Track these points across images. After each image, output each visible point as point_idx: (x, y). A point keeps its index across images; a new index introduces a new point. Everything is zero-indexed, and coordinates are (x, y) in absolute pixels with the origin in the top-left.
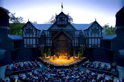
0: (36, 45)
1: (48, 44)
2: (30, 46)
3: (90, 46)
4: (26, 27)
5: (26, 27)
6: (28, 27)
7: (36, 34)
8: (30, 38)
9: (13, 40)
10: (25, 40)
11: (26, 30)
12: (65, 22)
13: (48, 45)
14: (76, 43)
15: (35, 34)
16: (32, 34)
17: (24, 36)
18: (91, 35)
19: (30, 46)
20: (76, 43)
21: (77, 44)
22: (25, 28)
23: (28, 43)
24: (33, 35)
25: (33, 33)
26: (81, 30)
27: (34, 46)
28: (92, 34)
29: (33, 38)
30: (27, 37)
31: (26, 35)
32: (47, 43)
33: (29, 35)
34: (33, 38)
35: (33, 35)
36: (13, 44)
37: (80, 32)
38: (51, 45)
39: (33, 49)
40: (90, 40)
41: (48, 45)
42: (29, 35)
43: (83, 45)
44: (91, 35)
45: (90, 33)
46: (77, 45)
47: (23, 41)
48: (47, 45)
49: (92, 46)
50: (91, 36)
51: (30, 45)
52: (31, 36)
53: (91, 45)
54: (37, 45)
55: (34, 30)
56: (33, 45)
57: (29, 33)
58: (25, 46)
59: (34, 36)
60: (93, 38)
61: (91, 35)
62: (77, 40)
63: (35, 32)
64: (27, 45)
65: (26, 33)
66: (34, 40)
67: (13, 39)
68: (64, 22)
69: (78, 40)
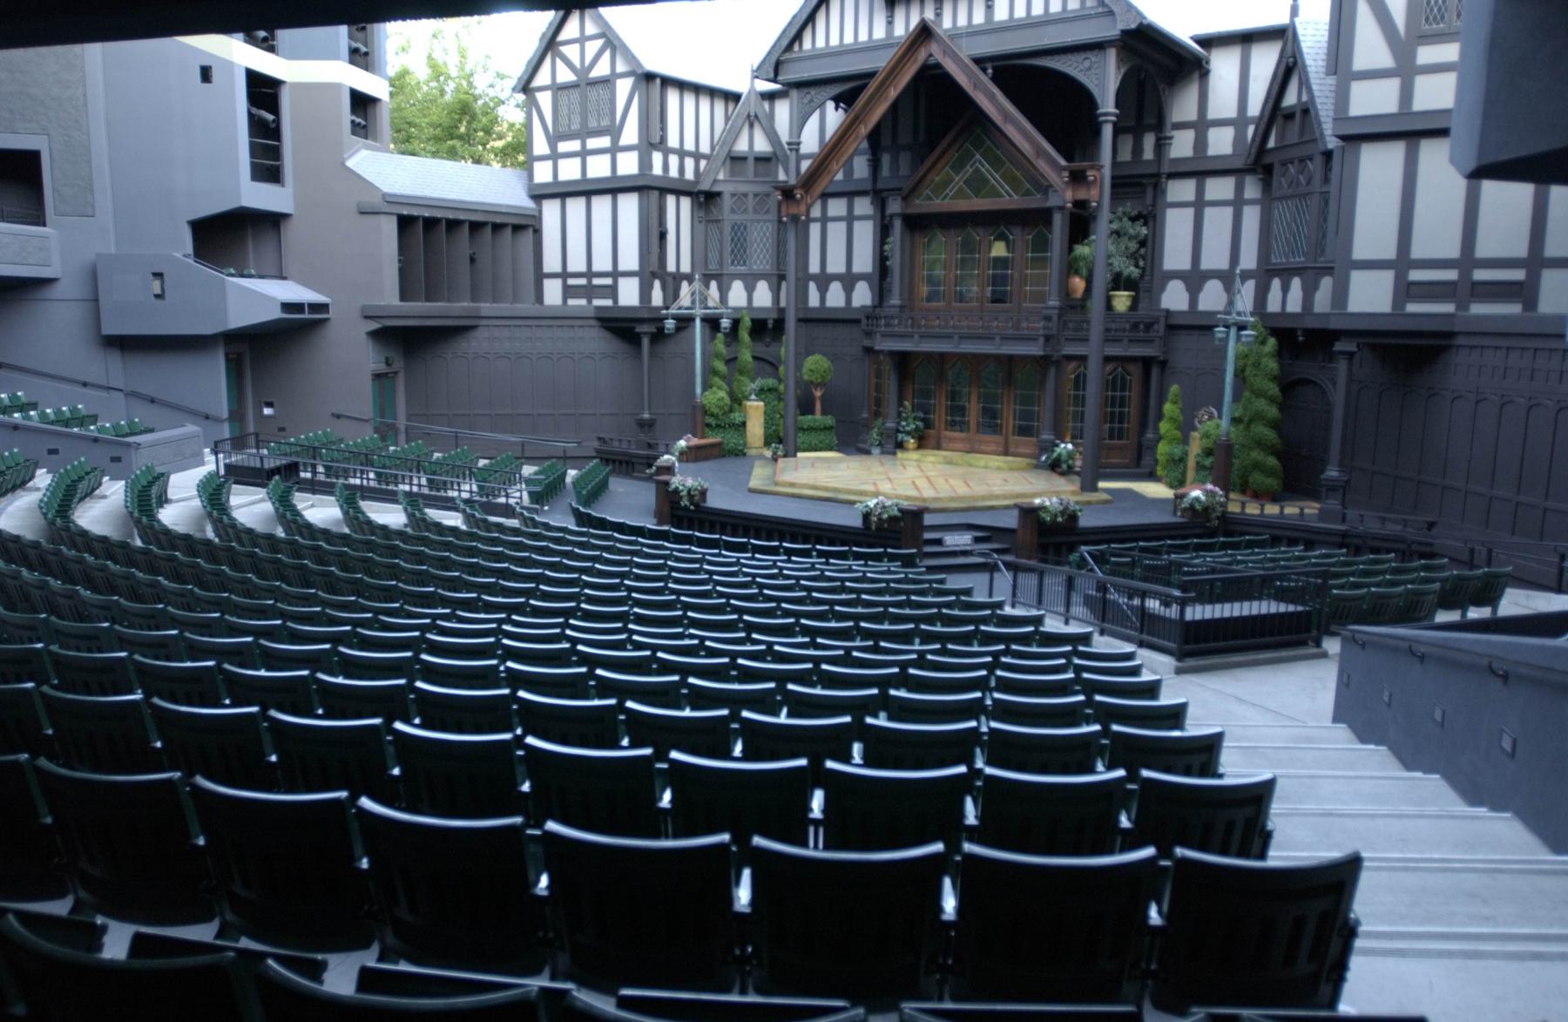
1: (824, 281)
2: (589, 292)
3: (1370, 295)
7: (653, 141)
9: (384, 195)
10: (550, 210)
11: (558, 89)
13: (823, 291)
15: (630, 135)
16: (1416, 275)
17: (543, 173)
22: (543, 78)
25: (615, 131)
26: (1281, 34)
27: (629, 294)
32: (814, 268)
33: (584, 154)
36: (390, 227)
37: (1265, 61)
38: (863, 296)
39: (624, 328)
40: (1378, 170)
41: (823, 291)
47: (525, 227)
48: (814, 300)
49: (1406, 291)
50: (1406, 94)
52: (599, 168)
53: (1388, 276)
55: (624, 87)
56: (615, 274)
57: (584, 134)
58: (553, 292)
61: (1392, 86)
65: (553, 140)
67: (386, 189)
69: (1251, 216)
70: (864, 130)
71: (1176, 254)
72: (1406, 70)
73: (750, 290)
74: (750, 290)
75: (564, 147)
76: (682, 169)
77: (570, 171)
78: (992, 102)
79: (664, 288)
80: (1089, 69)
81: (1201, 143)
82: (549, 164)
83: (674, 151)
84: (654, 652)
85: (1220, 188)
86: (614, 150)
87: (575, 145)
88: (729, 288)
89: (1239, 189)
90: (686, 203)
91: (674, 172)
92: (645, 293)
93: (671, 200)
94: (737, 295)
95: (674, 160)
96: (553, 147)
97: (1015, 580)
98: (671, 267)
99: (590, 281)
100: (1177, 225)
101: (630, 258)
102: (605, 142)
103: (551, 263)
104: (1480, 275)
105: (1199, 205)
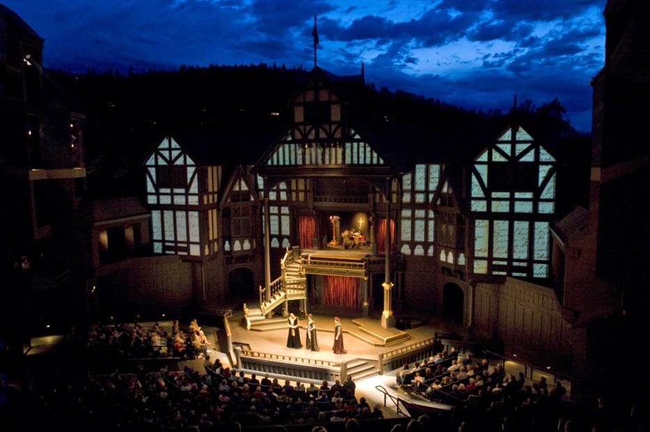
0: (204, 240)
2: (176, 249)
4: (509, 154)
5: (509, 154)
6: (525, 146)
8: (174, 208)
12: (334, 127)
13: (412, 249)
14: (422, 239)
15: (194, 188)
16: (494, 263)
18: (488, 199)
19: (176, 249)
20: (420, 237)
21: (426, 245)
23: (501, 251)
24: (187, 194)
25: (188, 187)
27: (195, 251)
28: (494, 195)
29: (187, 208)
30: (494, 210)
31: (158, 194)
33: (172, 194)
34: (187, 208)
35: (187, 194)
42: (172, 194)
43: (451, 255)
44: (484, 203)
45: (476, 191)
46: (426, 250)
50: (158, 199)
51: (176, 241)
52: (180, 200)
54: (210, 243)
59: (194, 200)
60: (180, 208)
61: (484, 203)
62: (426, 219)
63: (196, 180)
64: (163, 241)
65: (157, 187)
66: (194, 217)
68: (327, 127)
71: (406, 236)
72: (488, 199)
73: (242, 243)
74: (242, 243)
77: (165, 200)
81: (413, 198)
82: (161, 197)
83: (210, 193)
85: (420, 213)
88: (234, 244)
89: (427, 214)
92: (202, 250)
94: (237, 246)
99: (172, 191)
100: (406, 225)
101: (195, 236)
103: (157, 235)
104: (515, 264)
105: (413, 219)
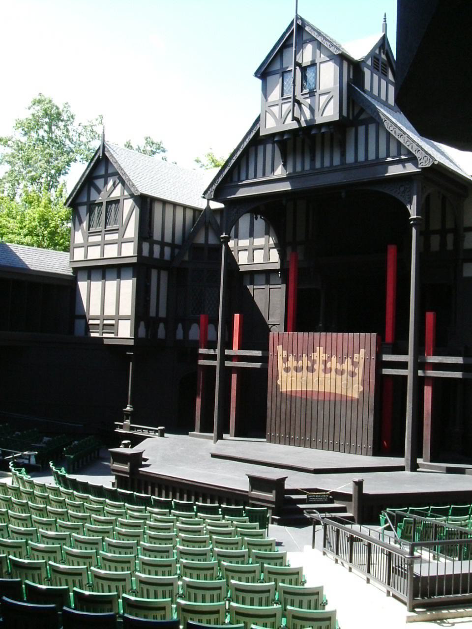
33: (104, 244)
52: (111, 252)
70: (439, 552)
75: (92, 239)
76: (151, 251)
78: (380, 69)
79: (166, 328)
80: (404, 192)
83: (157, 242)
84: (204, 519)
86: (120, 242)
87: (97, 239)
88: (190, 328)
90: (164, 275)
91: (157, 254)
93: (154, 273)
95: (157, 249)
96: (86, 239)
97: (347, 394)
98: (152, 313)
102: (115, 236)
